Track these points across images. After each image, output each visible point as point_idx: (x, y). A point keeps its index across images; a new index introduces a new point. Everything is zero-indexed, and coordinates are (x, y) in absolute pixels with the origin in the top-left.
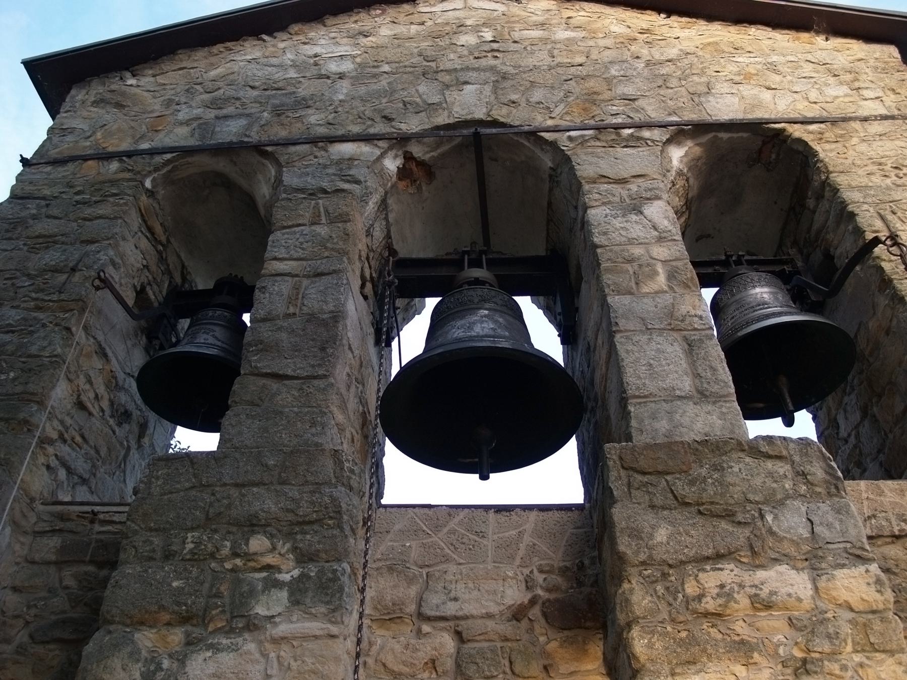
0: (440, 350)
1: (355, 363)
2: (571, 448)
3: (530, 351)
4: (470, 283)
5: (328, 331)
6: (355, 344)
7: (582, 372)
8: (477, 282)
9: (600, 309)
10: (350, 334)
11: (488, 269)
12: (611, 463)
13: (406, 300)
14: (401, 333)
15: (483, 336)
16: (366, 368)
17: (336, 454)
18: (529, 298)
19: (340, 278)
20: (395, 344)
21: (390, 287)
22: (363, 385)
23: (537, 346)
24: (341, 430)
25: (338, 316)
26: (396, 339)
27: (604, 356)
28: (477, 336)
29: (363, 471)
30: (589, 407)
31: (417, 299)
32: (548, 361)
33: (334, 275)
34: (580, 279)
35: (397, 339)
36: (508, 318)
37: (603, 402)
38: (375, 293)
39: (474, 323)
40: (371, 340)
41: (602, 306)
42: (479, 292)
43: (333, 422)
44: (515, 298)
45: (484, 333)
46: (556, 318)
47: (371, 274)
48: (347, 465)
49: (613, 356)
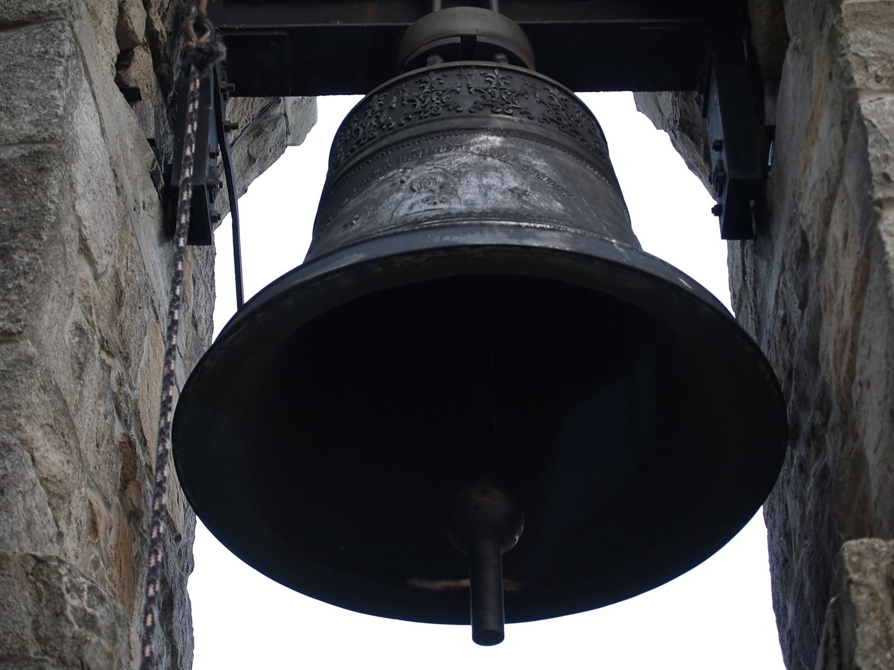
0: (356, 257)
1: (102, 296)
2: (746, 558)
3: (626, 260)
4: (449, 52)
5: (15, 198)
6: (100, 237)
7: (785, 321)
8: (471, 48)
9: (837, 131)
10: (84, 208)
11: (501, 11)
12: (861, 598)
13: (259, 103)
14: (242, 203)
15: (484, 215)
16: (135, 308)
17: (40, 569)
18: (628, 96)
19: (53, 38)
20: (222, 234)
21: (201, 66)
22: (126, 359)
23: (649, 246)
24: (58, 496)
25: (44, 153)
26: (227, 221)
27: (848, 275)
28: (469, 215)
29: (122, 621)
30: (805, 428)
31: (290, 100)
32: (679, 290)
33: (36, 29)
34: (780, 42)
35: (228, 220)
36: (560, 155)
37: (845, 414)
38: (163, 82)
39: (459, 174)
40: (149, 225)
41: (845, 123)
42: (476, 80)
43: (32, 474)
44: (587, 98)
45: (489, 205)
46: (707, 158)
47: (149, 22)
48: (72, 601)
49: (875, 276)
